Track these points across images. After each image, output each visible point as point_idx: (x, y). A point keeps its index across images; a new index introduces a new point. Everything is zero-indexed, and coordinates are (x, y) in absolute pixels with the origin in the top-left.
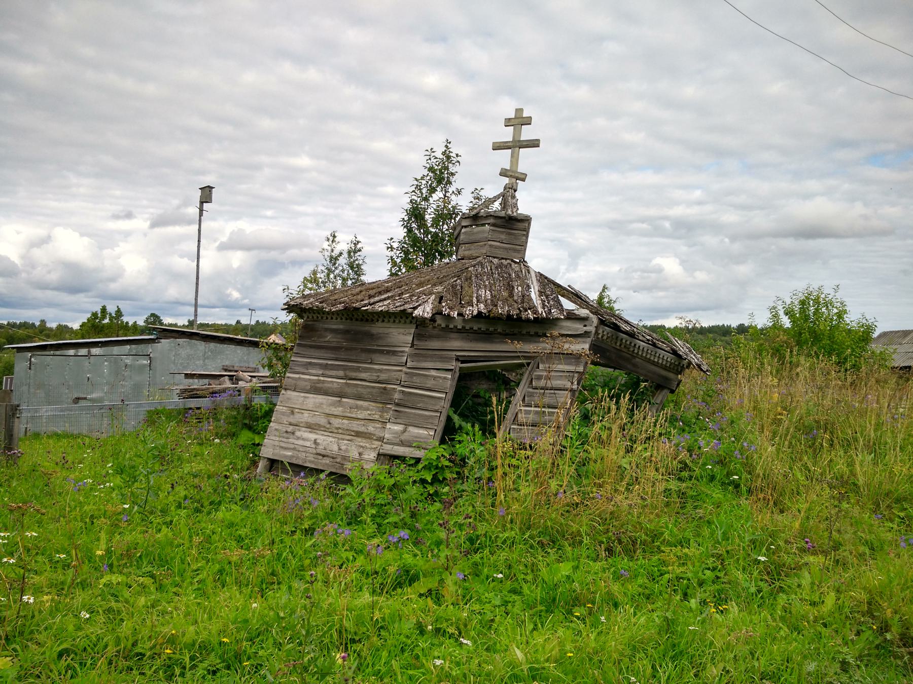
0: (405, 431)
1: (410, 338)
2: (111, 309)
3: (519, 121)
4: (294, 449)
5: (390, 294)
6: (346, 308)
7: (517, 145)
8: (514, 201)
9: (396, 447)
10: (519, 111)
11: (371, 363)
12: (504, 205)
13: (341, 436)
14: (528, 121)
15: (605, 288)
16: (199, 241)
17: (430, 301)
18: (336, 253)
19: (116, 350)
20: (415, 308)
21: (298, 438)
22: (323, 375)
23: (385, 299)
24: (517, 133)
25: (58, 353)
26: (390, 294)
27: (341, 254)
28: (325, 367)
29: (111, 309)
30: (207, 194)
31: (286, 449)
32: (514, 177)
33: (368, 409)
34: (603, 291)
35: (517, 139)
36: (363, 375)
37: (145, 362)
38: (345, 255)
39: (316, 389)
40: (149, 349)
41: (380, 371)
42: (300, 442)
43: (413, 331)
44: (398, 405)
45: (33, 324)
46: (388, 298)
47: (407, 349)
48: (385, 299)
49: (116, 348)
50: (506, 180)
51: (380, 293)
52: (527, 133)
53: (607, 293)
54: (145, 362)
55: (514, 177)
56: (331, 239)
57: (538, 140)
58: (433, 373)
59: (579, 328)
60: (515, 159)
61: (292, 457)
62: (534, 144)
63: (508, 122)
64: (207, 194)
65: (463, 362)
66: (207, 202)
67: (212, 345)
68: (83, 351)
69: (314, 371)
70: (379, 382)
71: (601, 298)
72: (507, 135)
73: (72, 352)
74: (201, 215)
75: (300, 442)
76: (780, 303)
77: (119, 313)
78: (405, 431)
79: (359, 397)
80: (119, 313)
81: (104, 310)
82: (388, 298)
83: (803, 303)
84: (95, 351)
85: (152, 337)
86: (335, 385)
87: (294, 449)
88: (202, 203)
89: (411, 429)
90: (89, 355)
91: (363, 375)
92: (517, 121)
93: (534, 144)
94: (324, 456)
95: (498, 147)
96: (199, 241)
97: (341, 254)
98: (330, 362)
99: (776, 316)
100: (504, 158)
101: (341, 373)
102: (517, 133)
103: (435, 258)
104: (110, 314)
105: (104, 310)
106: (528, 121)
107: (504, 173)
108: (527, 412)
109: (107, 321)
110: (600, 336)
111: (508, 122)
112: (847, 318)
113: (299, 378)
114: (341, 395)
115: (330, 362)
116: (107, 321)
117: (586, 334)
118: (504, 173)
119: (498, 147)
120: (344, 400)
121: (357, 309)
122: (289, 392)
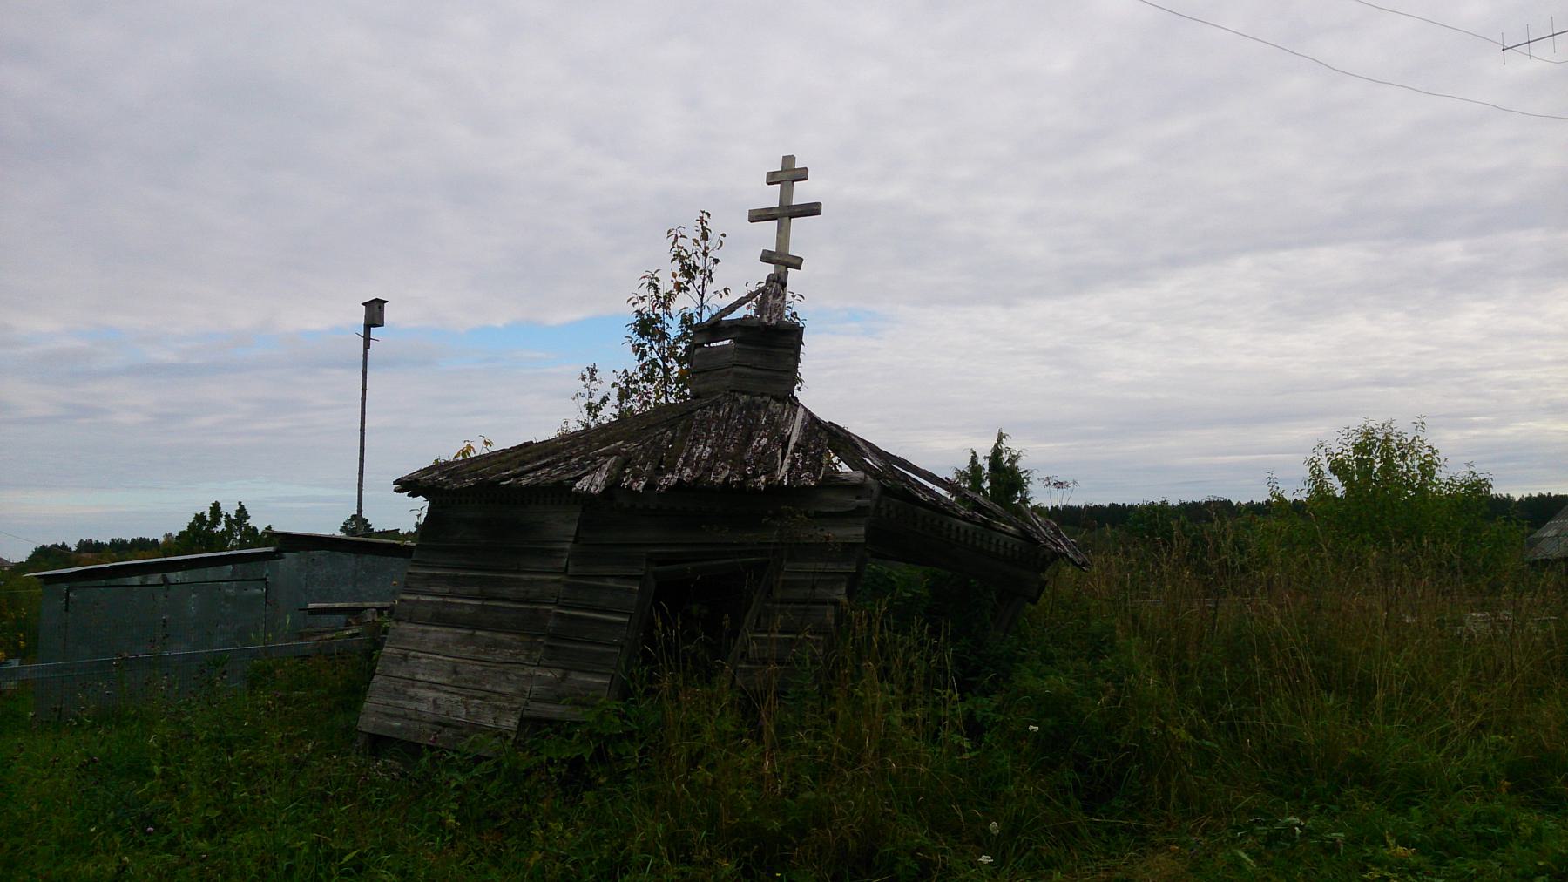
0: (564, 678)
1: (573, 528)
2: (229, 509)
3: (788, 174)
4: (404, 717)
5: (550, 459)
6: (477, 484)
7: (786, 213)
8: (778, 301)
9: (1355, 324)
10: (788, 160)
11: (518, 571)
12: (761, 308)
13: (470, 692)
14: (802, 175)
17: (606, 467)
18: (596, 400)
19: (210, 573)
20: (578, 479)
21: (411, 698)
22: (451, 595)
23: (541, 467)
24: (786, 194)
25: (113, 582)
26: (550, 459)
27: (605, 400)
28: (455, 581)
29: (229, 509)
31: (393, 716)
33: (510, 647)
34: (999, 441)
36: (507, 592)
37: (258, 591)
38: (614, 400)
39: (441, 618)
40: (266, 569)
41: (531, 582)
42: (413, 705)
43: (577, 515)
44: (552, 636)
45: (155, 541)
46: (546, 465)
47: (567, 546)
48: (541, 467)
49: (210, 570)
50: (770, 269)
51: (540, 458)
52: (802, 193)
53: (1006, 443)
54: (258, 591)
55: (782, 261)
56: (588, 375)
57: (819, 204)
58: (611, 583)
59: (851, 502)
60: (783, 235)
61: (401, 728)
62: (813, 210)
63: (772, 178)
64: (375, 312)
65: (659, 563)
67: (367, 559)
68: (155, 578)
69: (437, 589)
70: (527, 602)
71: (997, 452)
72: (770, 197)
73: (136, 580)
74: (367, 346)
75: (413, 705)
76: (1322, 451)
77: (242, 513)
78: (564, 678)
79: (498, 627)
80: (242, 513)
81: (216, 509)
82: (546, 465)
83: (1358, 448)
84: (174, 576)
85: (271, 549)
86: (467, 610)
87: (404, 717)
88: (368, 327)
89: (573, 675)
90: (166, 581)
91: (507, 592)
92: (785, 176)
93: (813, 210)
94: (445, 726)
95: (757, 216)
96: (364, 390)
97: (605, 400)
98: (461, 573)
99: (1317, 476)
101: (476, 590)
102: (786, 194)
104: (228, 516)
105: (216, 509)
107: (767, 257)
108: (761, 642)
109: (221, 527)
110: (884, 514)
111: (772, 178)
112: (1442, 475)
113: (418, 601)
114: (475, 625)
115: (461, 573)
116: (221, 527)
117: (860, 512)
118: (767, 257)
119: (757, 216)
120: (478, 633)
121: (494, 484)
122: (403, 625)
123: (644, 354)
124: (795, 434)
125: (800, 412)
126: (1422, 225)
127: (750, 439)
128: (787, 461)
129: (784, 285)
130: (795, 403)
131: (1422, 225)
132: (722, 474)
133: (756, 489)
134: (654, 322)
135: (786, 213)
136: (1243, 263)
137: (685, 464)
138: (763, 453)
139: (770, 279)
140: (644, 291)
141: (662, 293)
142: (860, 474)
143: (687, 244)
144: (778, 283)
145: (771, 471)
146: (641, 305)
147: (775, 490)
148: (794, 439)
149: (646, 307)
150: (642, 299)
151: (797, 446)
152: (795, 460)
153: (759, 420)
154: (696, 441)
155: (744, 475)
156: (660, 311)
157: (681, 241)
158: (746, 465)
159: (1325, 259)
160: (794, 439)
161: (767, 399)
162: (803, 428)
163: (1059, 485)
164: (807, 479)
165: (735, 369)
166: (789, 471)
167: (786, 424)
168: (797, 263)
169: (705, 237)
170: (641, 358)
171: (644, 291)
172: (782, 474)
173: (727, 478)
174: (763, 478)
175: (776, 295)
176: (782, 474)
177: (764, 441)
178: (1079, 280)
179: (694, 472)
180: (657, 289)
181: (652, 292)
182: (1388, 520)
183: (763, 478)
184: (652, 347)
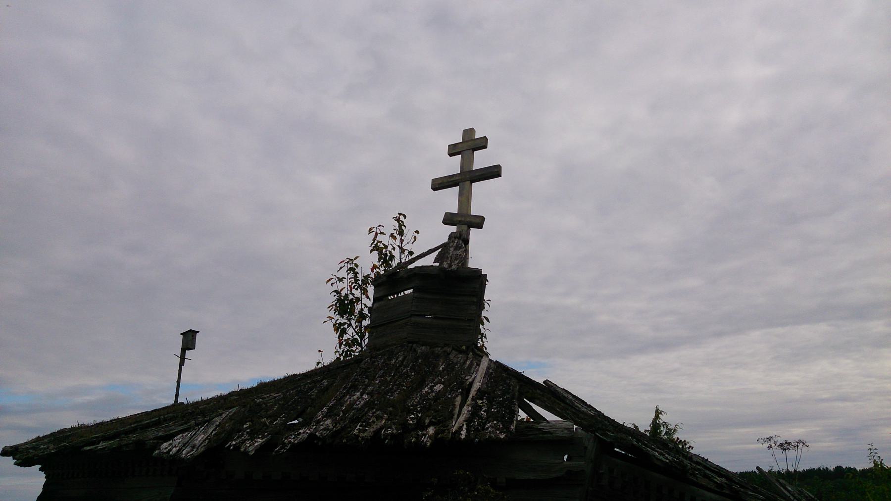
3: (471, 144)
7: (465, 179)
9: (822, 367)
10: (469, 133)
14: (482, 144)
15: (658, 413)
16: (178, 382)
30: (189, 339)
32: (464, 222)
35: (466, 169)
52: (481, 160)
53: (663, 418)
55: (464, 222)
57: (482, 219)
60: (465, 199)
62: (493, 172)
63: (453, 150)
64: (189, 339)
66: (189, 349)
71: (656, 425)
72: (453, 166)
88: (183, 351)
93: (493, 172)
95: (439, 185)
96: (178, 382)
100: (450, 200)
102: (467, 162)
103: (356, 390)
106: (482, 144)
107: (449, 219)
111: (453, 150)
118: (449, 219)
119: (439, 185)
123: (344, 332)
124: (478, 381)
125: (484, 363)
126: (861, 312)
127: (422, 384)
128: (466, 409)
129: (466, 242)
130: (481, 353)
131: (861, 312)
132: (379, 424)
133: (419, 445)
134: (352, 302)
135: (465, 179)
136: (755, 334)
137: (327, 416)
138: (436, 399)
139: (452, 236)
140: (343, 273)
141: (360, 277)
142: (568, 424)
143: (385, 240)
144: (460, 242)
145: (442, 422)
146: (340, 286)
147: (447, 445)
148: (477, 386)
149: (344, 287)
150: (341, 280)
151: (481, 393)
152: (476, 409)
153: (436, 366)
154: (354, 388)
155: (404, 426)
156: (357, 293)
157: (380, 238)
158: (409, 412)
159: (808, 333)
160: (477, 386)
161: (449, 350)
162: (488, 374)
163: (785, 446)
164: (494, 431)
165: (413, 319)
166: (469, 421)
167: (469, 371)
168: (479, 223)
169: (401, 233)
170: (341, 336)
171: (343, 273)
172: (459, 424)
173: (378, 431)
174: (431, 430)
175: (457, 248)
176: (459, 424)
177: (439, 387)
178: (663, 345)
179: (335, 423)
180: (356, 274)
181: (351, 275)
182: (879, 475)
183: (431, 430)
184: (350, 325)
